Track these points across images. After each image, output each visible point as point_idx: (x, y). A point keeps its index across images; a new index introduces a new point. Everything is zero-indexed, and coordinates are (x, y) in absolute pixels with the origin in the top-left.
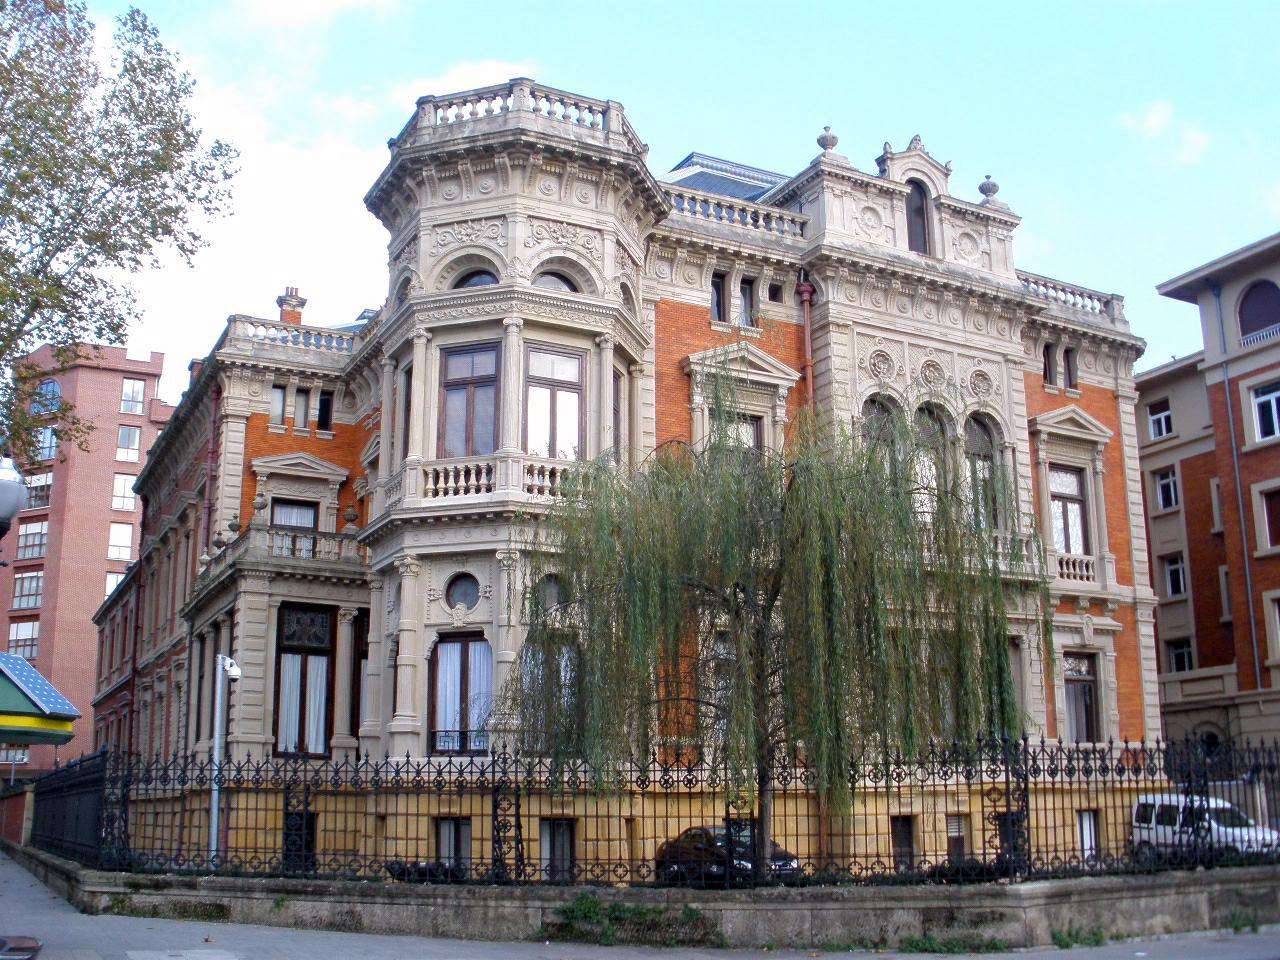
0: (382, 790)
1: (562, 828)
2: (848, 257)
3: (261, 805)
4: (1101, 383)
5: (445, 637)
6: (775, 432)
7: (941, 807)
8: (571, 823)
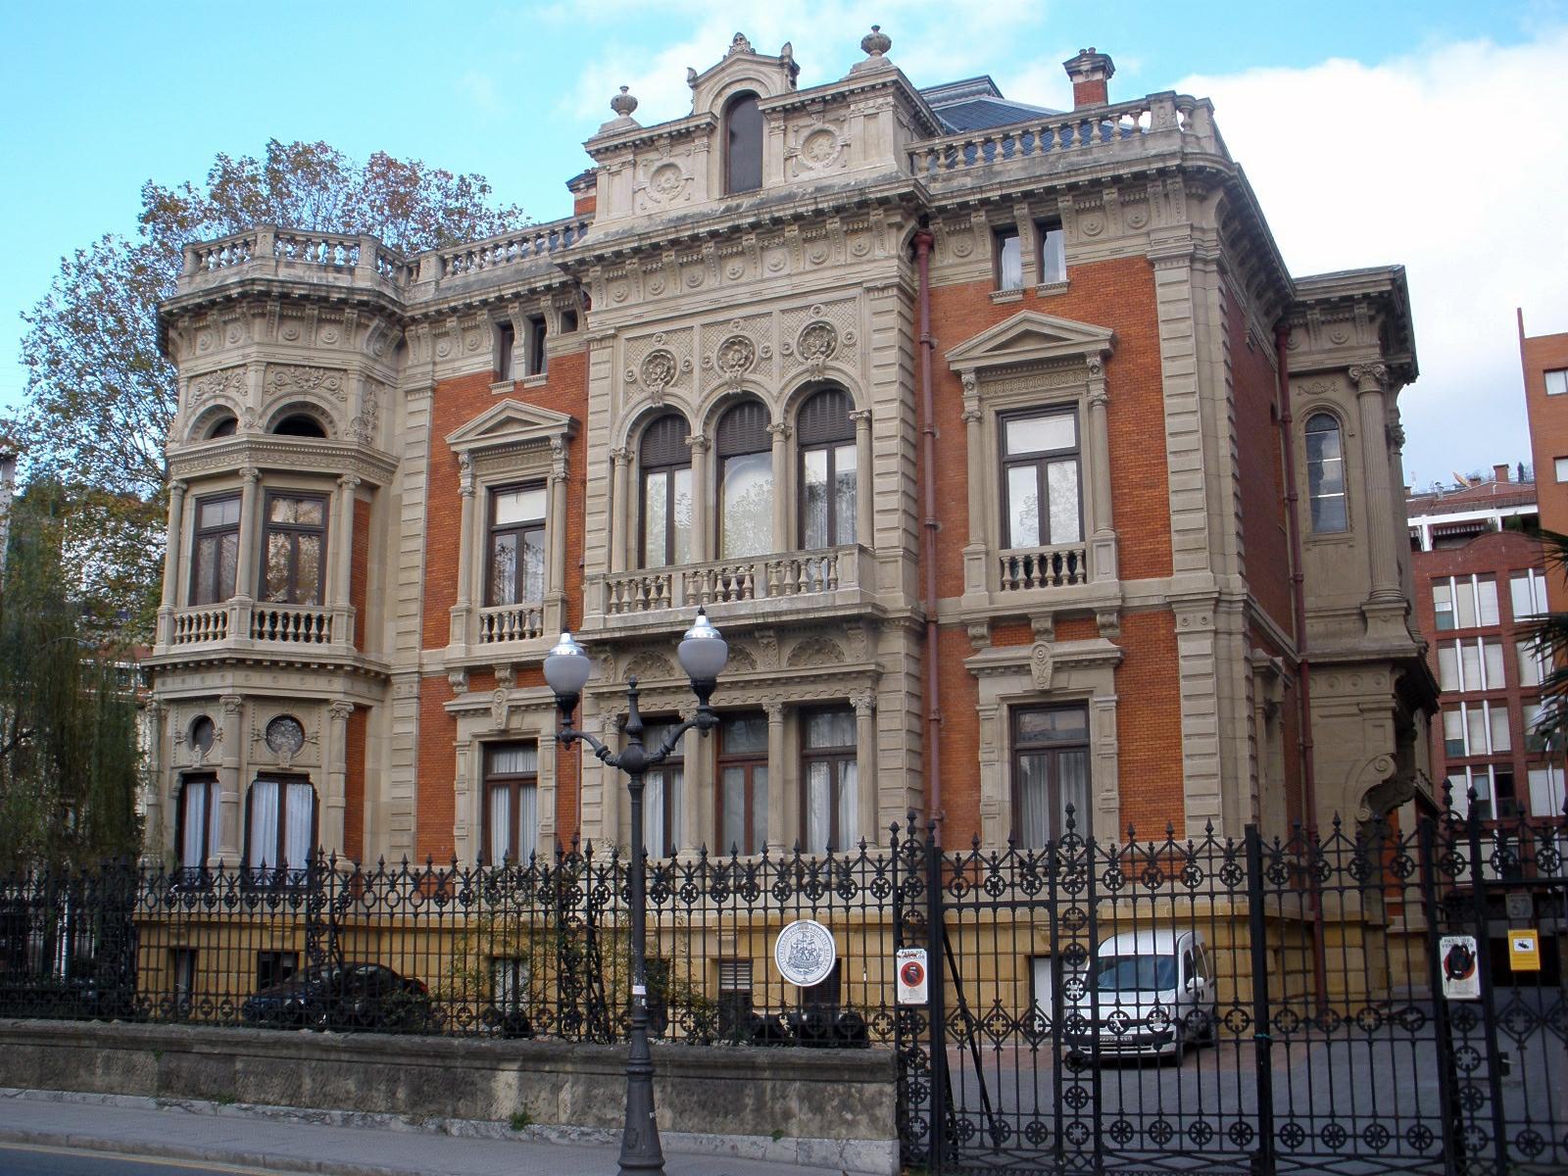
0: (379, 932)
1: (184, 957)
2: (587, 255)
3: (224, 944)
4: (1120, 250)
5: (264, 777)
6: (981, 434)
7: (697, 948)
8: (193, 954)
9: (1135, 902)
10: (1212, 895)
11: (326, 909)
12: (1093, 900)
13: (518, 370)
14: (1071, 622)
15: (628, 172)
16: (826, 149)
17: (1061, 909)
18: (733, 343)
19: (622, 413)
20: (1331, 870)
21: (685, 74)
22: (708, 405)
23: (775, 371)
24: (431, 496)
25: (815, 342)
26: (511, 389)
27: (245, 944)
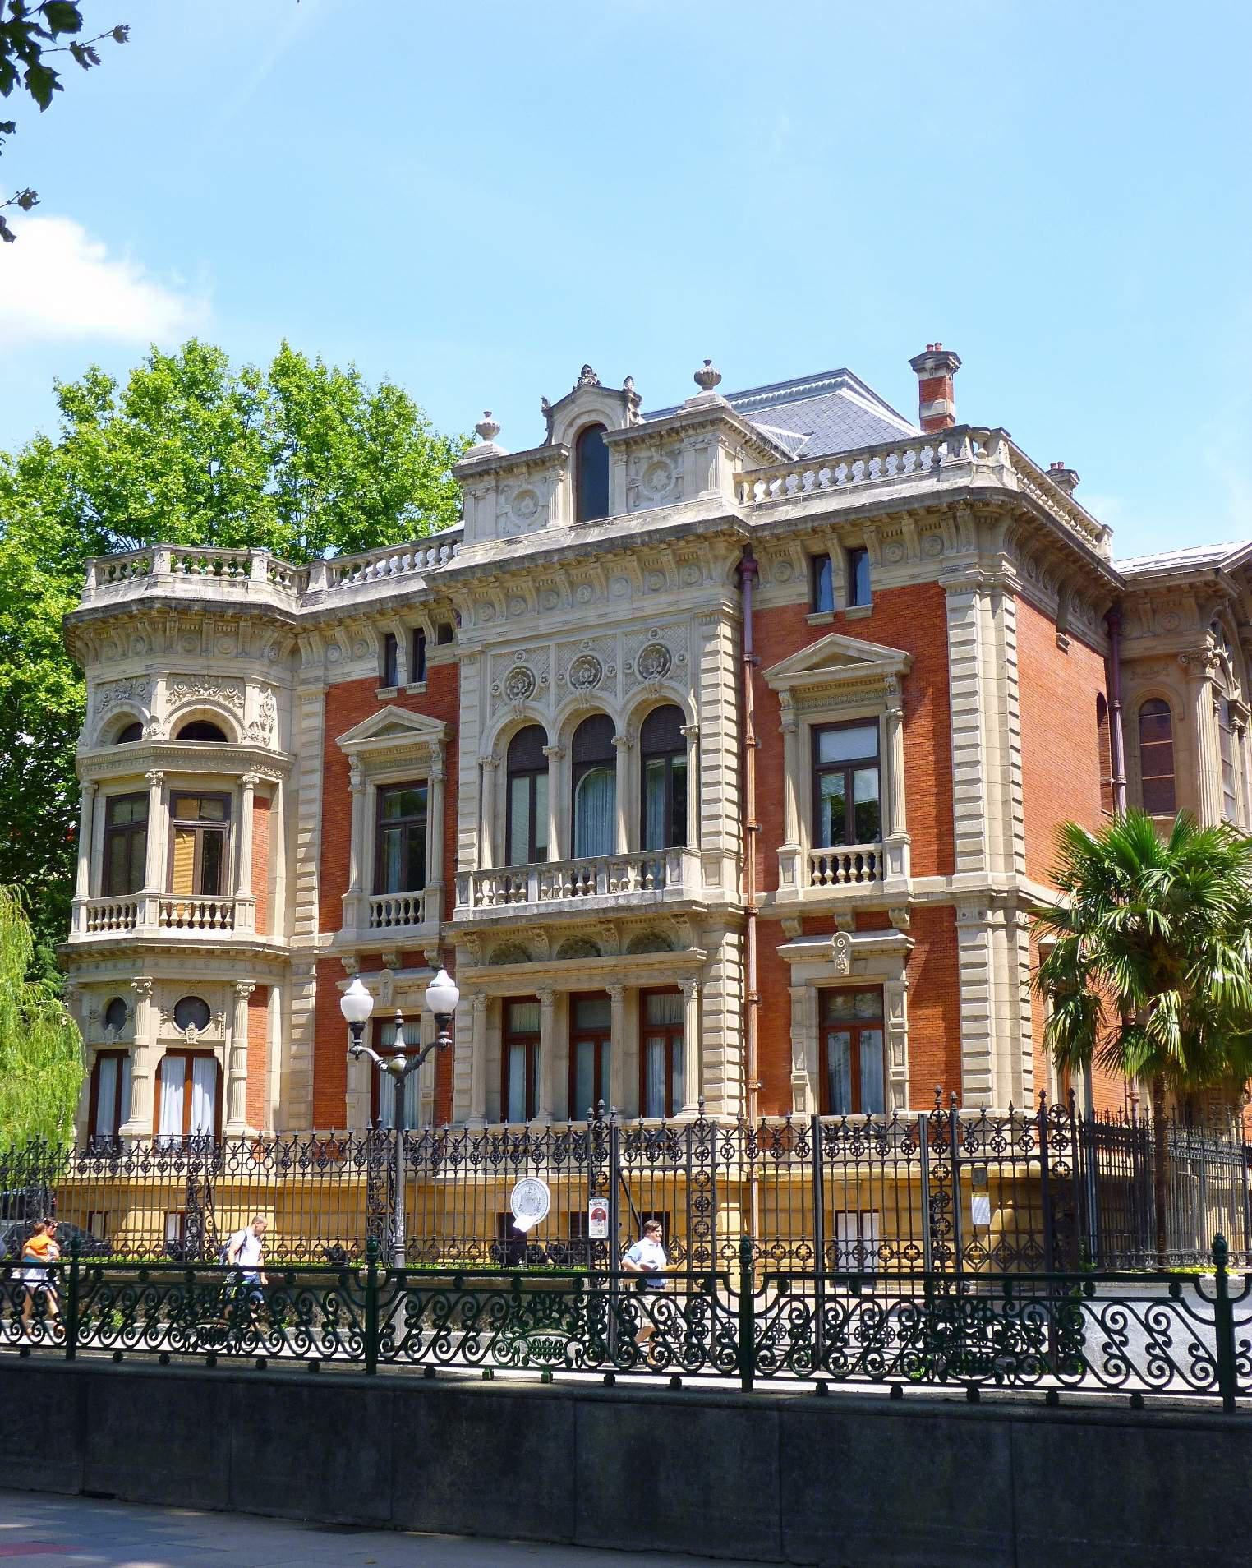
9: (896, 1164)
10: (845, 1164)
11: (202, 1172)
12: (715, 1166)
13: (402, 677)
14: (869, 919)
15: (491, 496)
16: (665, 481)
17: (695, 1171)
18: (584, 663)
19: (489, 723)
20: (1006, 1144)
21: (540, 405)
22: (562, 718)
23: (619, 688)
24: (326, 791)
25: (584, 674)
26: (395, 695)
27: (481, 1208)
